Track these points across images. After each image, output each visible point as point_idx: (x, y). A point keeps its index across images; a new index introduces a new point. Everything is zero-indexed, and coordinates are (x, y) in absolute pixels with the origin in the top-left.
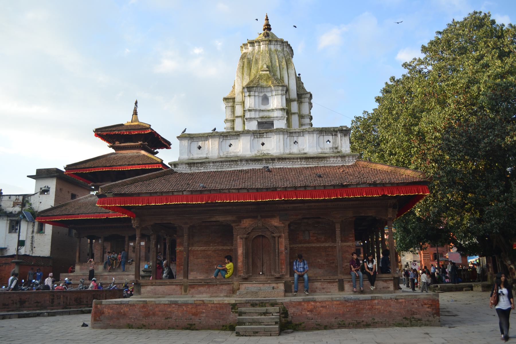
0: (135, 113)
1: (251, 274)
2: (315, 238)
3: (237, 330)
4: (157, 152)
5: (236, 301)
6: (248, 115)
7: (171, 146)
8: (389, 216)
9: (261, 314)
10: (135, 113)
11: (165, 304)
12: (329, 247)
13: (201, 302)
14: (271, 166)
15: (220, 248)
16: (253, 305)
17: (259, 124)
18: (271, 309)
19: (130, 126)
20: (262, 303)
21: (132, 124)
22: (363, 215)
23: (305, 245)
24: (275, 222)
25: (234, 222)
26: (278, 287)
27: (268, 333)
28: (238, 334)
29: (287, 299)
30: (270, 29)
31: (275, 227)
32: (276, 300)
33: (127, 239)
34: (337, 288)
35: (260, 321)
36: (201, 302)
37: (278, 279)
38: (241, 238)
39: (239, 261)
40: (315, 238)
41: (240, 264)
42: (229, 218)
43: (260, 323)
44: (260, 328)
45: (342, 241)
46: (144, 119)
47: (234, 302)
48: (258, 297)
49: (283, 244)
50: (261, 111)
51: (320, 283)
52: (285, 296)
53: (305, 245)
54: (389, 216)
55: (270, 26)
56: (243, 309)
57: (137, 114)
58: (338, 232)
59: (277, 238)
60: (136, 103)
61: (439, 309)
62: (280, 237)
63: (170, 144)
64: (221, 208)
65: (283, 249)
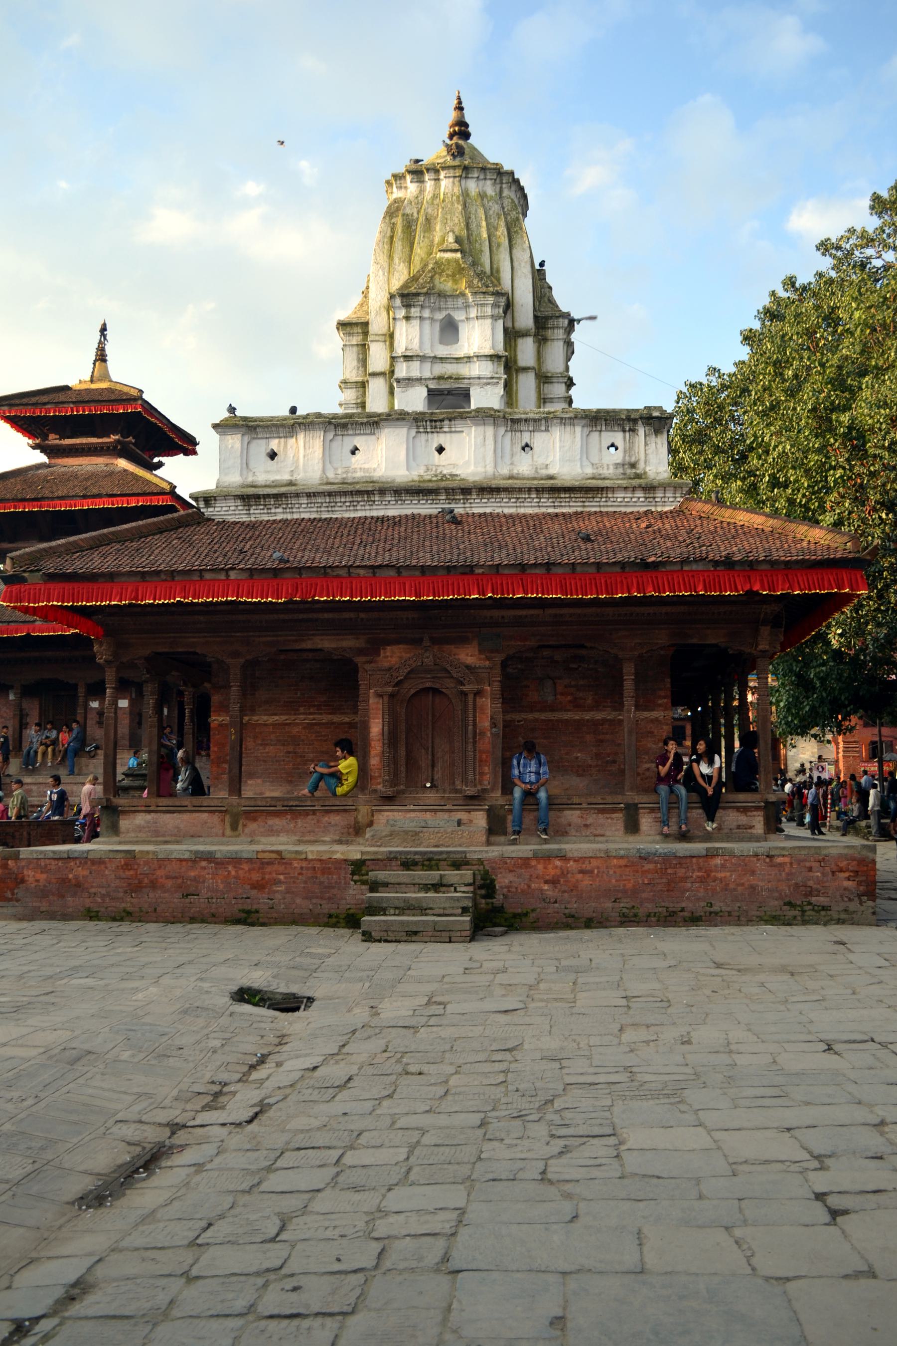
0: (101, 357)
1: (402, 787)
2: (569, 698)
4: (160, 465)
5: (362, 853)
6: (402, 370)
7: (198, 448)
9: (426, 888)
10: (101, 357)
12: (604, 721)
13: (274, 856)
14: (459, 509)
15: (325, 718)
17: (431, 393)
22: (695, 641)
23: (543, 716)
25: (361, 652)
26: (471, 821)
29: (494, 852)
31: (468, 667)
33: (81, 691)
34: (620, 825)
36: (274, 856)
37: (473, 801)
39: (373, 752)
40: (569, 698)
42: (348, 643)
45: (638, 707)
46: (125, 372)
47: (358, 857)
49: (487, 711)
52: (489, 843)
54: (761, 647)
55: (467, 125)
56: (381, 875)
57: (105, 361)
58: (629, 685)
59: (471, 697)
60: (103, 329)
62: (478, 693)
64: (326, 616)
65: (487, 724)
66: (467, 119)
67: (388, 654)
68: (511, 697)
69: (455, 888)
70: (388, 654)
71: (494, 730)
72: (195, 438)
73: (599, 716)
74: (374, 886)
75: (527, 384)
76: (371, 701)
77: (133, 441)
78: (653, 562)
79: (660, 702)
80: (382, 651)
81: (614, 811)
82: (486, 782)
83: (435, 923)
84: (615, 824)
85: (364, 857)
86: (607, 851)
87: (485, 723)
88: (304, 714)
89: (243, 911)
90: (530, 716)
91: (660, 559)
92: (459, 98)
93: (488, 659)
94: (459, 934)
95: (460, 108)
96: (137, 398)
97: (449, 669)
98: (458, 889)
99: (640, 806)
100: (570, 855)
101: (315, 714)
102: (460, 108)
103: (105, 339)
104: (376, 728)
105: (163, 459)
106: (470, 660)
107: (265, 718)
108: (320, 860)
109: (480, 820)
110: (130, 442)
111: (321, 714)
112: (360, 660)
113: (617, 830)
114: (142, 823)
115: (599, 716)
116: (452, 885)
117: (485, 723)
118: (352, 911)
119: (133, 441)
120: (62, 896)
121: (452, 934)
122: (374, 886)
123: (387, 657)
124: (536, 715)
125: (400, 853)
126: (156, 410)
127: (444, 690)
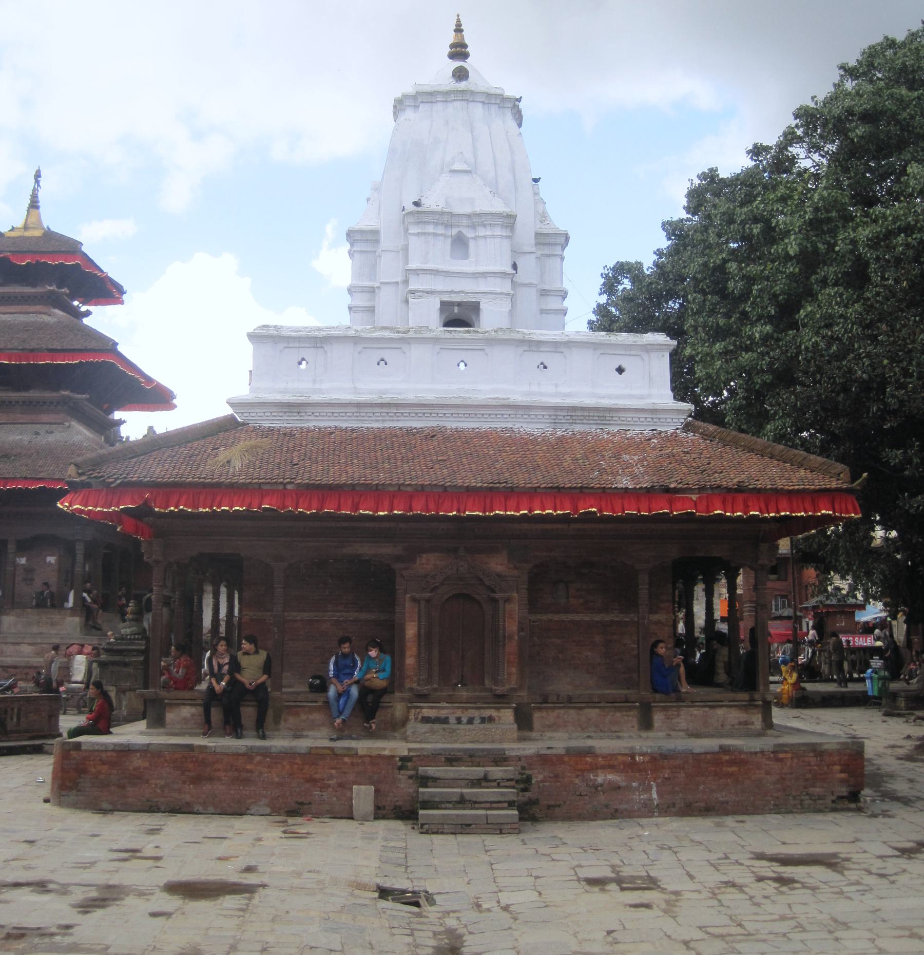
0: (34, 204)
1: (435, 686)
2: (581, 601)
3: (421, 821)
4: (88, 314)
5: (410, 750)
6: (415, 284)
7: (124, 297)
8: (760, 562)
10: (34, 204)
11: (238, 755)
12: (612, 622)
13: (328, 752)
15: (353, 615)
16: (452, 760)
18: (496, 772)
19: (23, 239)
20: (471, 756)
21: (27, 234)
22: (702, 554)
23: (556, 617)
24: (498, 564)
26: (500, 718)
27: (499, 829)
28: (427, 830)
29: (529, 749)
30: (464, 56)
31: (499, 575)
32: (504, 750)
33: (11, 547)
34: (634, 722)
35: (474, 799)
36: (328, 752)
37: (500, 700)
38: (414, 600)
39: (408, 653)
40: (581, 601)
41: (410, 661)
42: (387, 550)
43: (474, 804)
44: (476, 816)
47: (406, 753)
48: (455, 742)
49: (513, 615)
50: (447, 274)
51: (597, 710)
52: (521, 739)
53: (556, 617)
54: (760, 562)
55: (466, 46)
56: (431, 771)
57: (38, 208)
59: (501, 604)
60: (38, 175)
61: (863, 775)
62: (508, 600)
63: (121, 291)
65: (515, 628)
66: (467, 41)
67: (424, 561)
68: (533, 604)
69: (499, 784)
70: (424, 561)
71: (522, 634)
72: (122, 287)
73: (607, 618)
74: (425, 781)
75: (528, 297)
76: (407, 605)
77: (68, 291)
78: (675, 488)
79: (663, 605)
80: (418, 559)
81: (630, 709)
82: (513, 682)
83: (487, 816)
84: (631, 719)
85: (412, 754)
86: (631, 748)
87: (512, 627)
88: (331, 611)
89: (298, 803)
90: (544, 617)
91: (680, 486)
92: (459, 21)
93: (516, 568)
94: (509, 826)
95: (459, 30)
96: (72, 248)
97: (482, 577)
98: (502, 784)
99: (653, 704)
100: (598, 752)
101: (342, 611)
102: (459, 30)
103: (39, 185)
104: (411, 631)
105: (91, 308)
106: (500, 569)
107: (294, 614)
108: (370, 756)
109: (507, 715)
110: (65, 293)
111: (349, 612)
112: (397, 566)
113: (633, 727)
114: (189, 715)
115: (607, 618)
116: (495, 780)
117: (512, 627)
118: (400, 803)
119: (68, 291)
120: (123, 787)
121: (503, 827)
122: (425, 781)
123: (423, 564)
124: (550, 616)
125: (445, 750)
126: (92, 261)
127: (476, 597)
